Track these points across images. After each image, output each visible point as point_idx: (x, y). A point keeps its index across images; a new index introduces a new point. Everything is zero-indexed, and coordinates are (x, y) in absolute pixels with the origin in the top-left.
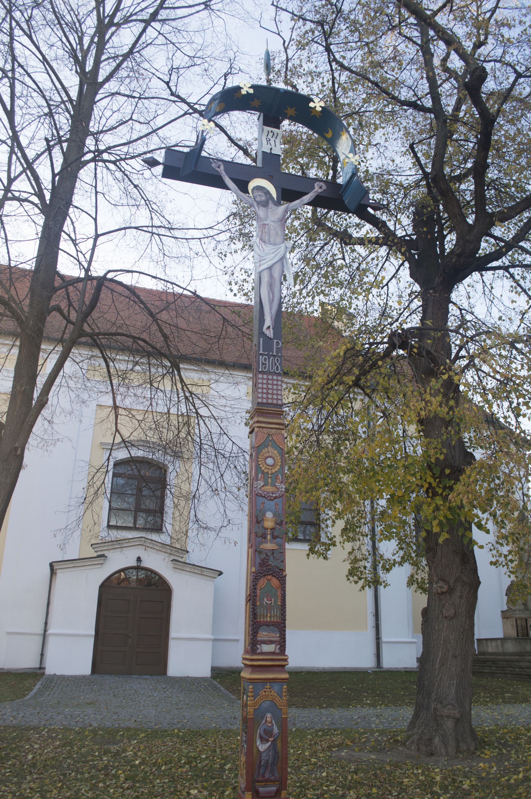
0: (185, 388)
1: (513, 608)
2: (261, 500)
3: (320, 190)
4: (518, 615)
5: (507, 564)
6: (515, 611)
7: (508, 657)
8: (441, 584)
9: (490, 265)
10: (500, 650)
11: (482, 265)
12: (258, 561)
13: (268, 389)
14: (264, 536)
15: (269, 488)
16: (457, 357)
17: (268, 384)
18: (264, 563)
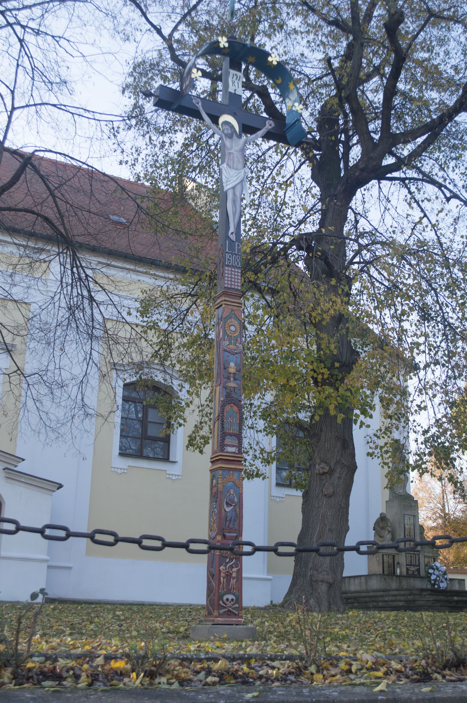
0: (75, 269)
2: (227, 354)
3: (270, 127)
5: (382, 455)
7: (371, 594)
8: (323, 465)
9: (389, 175)
10: (364, 587)
11: (381, 174)
12: (225, 393)
13: (231, 278)
14: (228, 378)
15: (232, 347)
16: (351, 263)
17: (231, 274)
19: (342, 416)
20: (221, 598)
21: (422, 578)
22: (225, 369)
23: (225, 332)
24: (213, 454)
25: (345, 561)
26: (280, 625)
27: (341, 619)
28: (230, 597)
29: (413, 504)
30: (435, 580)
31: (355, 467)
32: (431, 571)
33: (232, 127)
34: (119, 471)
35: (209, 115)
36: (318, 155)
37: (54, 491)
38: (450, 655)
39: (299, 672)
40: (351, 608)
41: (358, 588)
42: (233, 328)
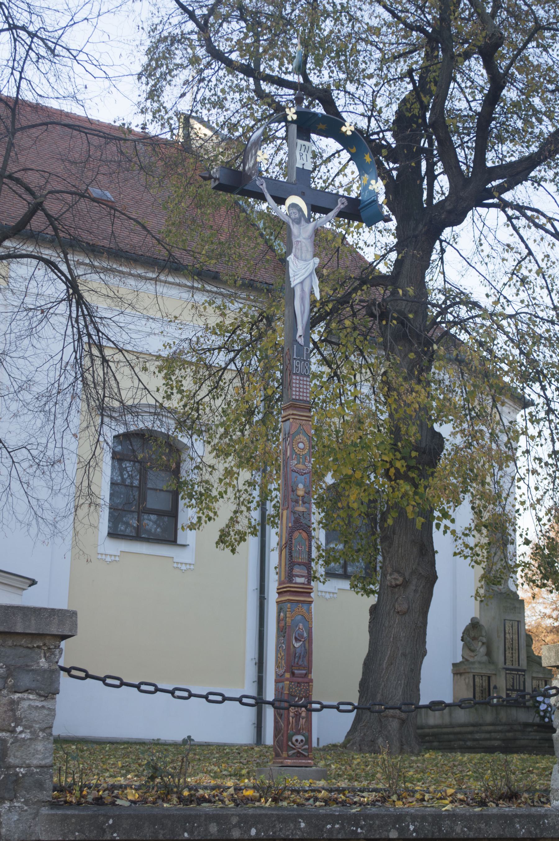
1: (471, 660)
2: (295, 474)
3: (342, 206)
4: (478, 669)
6: (473, 663)
7: (457, 729)
8: (396, 575)
10: (447, 720)
12: (293, 519)
13: (300, 388)
14: (297, 502)
15: (300, 466)
18: (297, 521)
19: (423, 520)
20: (290, 739)
21: (528, 707)
22: (293, 491)
23: (292, 449)
24: (280, 584)
25: (421, 692)
26: (348, 768)
27: (416, 762)
28: (300, 738)
29: (518, 606)
30: (545, 711)
31: (435, 578)
32: (540, 699)
33: (300, 210)
34: (108, 559)
35: (274, 197)
36: (393, 169)
37: (24, 589)
38: (505, 790)
39: (384, 800)
40: (428, 749)
41: (438, 721)
42: (301, 445)
